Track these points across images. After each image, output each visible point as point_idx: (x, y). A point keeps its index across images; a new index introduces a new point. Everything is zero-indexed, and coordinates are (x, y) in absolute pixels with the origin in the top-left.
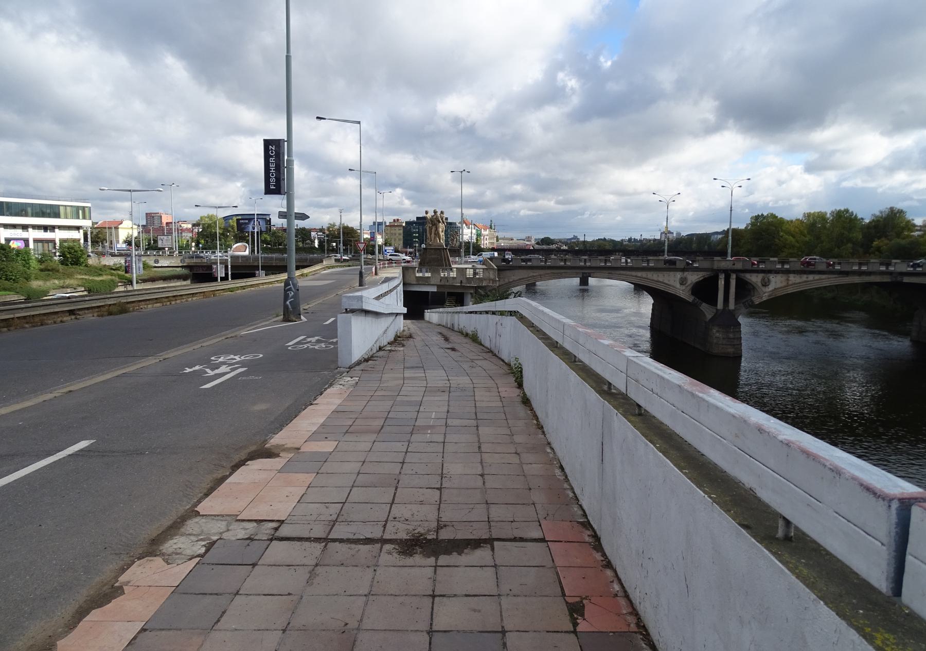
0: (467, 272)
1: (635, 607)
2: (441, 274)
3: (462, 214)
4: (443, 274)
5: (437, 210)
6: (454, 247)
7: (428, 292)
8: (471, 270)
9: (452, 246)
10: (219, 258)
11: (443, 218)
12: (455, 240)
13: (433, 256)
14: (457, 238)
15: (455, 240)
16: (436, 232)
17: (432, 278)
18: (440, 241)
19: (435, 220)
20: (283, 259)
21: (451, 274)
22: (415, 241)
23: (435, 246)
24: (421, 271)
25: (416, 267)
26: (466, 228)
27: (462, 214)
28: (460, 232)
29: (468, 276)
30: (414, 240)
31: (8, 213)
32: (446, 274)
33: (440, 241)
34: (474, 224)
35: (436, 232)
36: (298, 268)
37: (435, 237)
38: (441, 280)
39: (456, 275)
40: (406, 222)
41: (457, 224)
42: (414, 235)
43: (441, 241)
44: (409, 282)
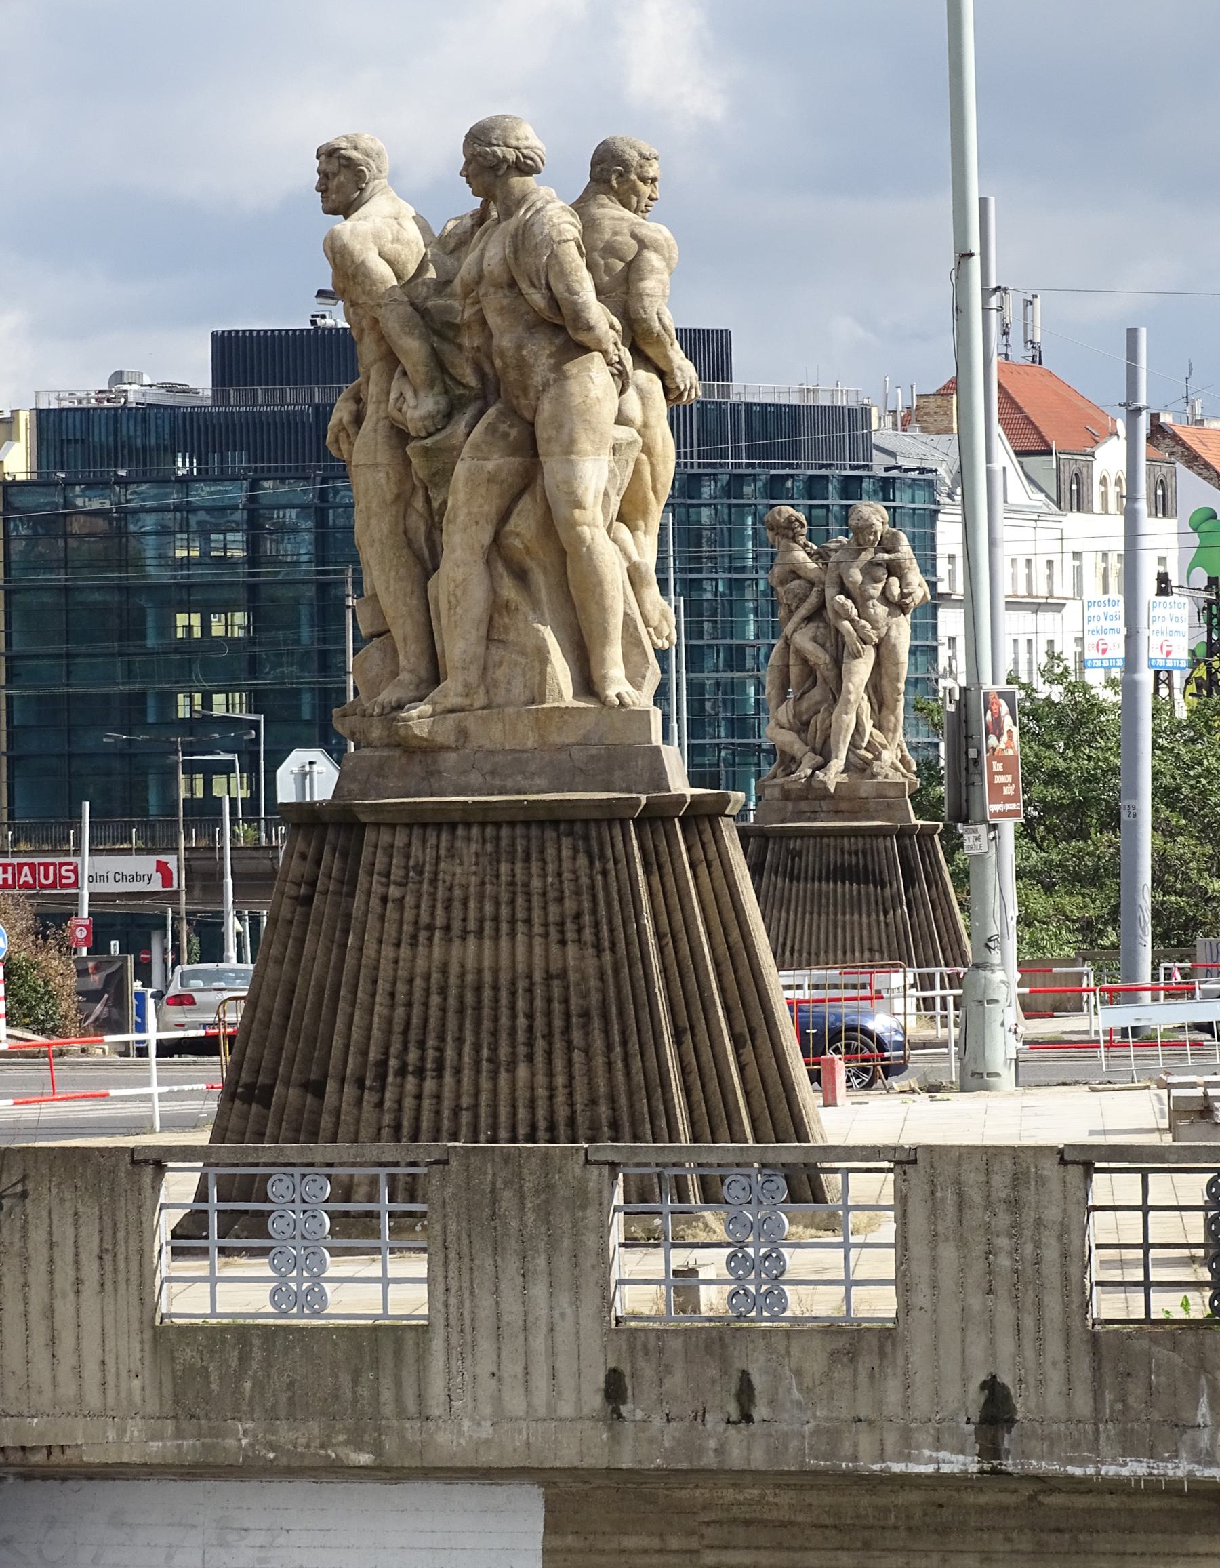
0: (1101, 1228)
1: (596, 677)
2: (627, 1263)
4: (651, 1263)
6: (842, 803)
8: (1162, 1188)
9: (813, 793)
11: (633, 271)
12: (861, 670)
14: (883, 648)
15: (861, 670)
16: (523, 524)
17: (464, 1350)
18: (588, 684)
19: (493, 304)
21: (797, 1261)
22: (203, 723)
24: (257, 1224)
26: (1018, 491)
28: (926, 547)
29: (1107, 1306)
30: (179, 635)
31: (839, 1150)
32: (712, 1263)
33: (588, 684)
34: (1158, 431)
35: (523, 524)
37: (497, 608)
39: (903, 1283)
40: (42, 416)
41: (882, 431)
42: (186, 622)
43: (617, 682)
44: (36, 1430)
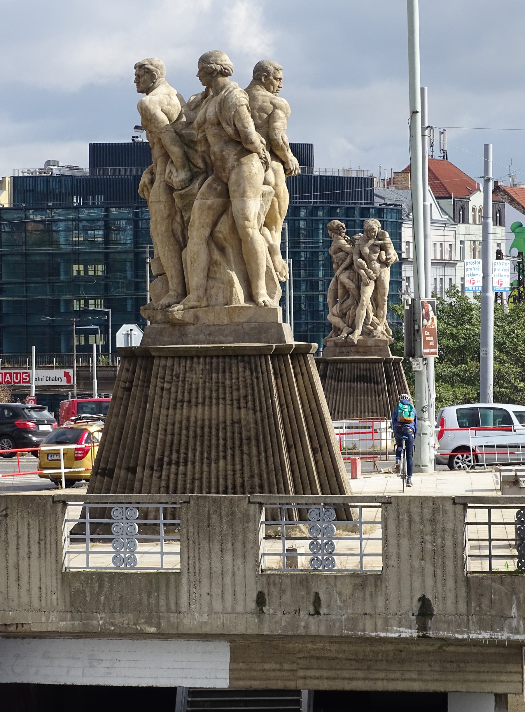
0: (471, 532)
2: (266, 546)
3: (243, 105)
4: (277, 546)
5: (226, 60)
6: (359, 348)
7: (171, 691)
8: (497, 515)
10: (76, 399)
11: (271, 118)
13: (198, 412)
15: (369, 291)
16: (223, 227)
17: (196, 583)
19: (211, 132)
20: (485, 422)
21: (340, 546)
23: (211, 336)
24: (107, 529)
25: (64, 502)
27: (243, 105)
29: (473, 565)
32: (303, 546)
35: (223, 227)
36: (299, 509)
37: (212, 263)
38: (261, 600)
39: (385, 555)
41: (378, 188)
43: (263, 296)
